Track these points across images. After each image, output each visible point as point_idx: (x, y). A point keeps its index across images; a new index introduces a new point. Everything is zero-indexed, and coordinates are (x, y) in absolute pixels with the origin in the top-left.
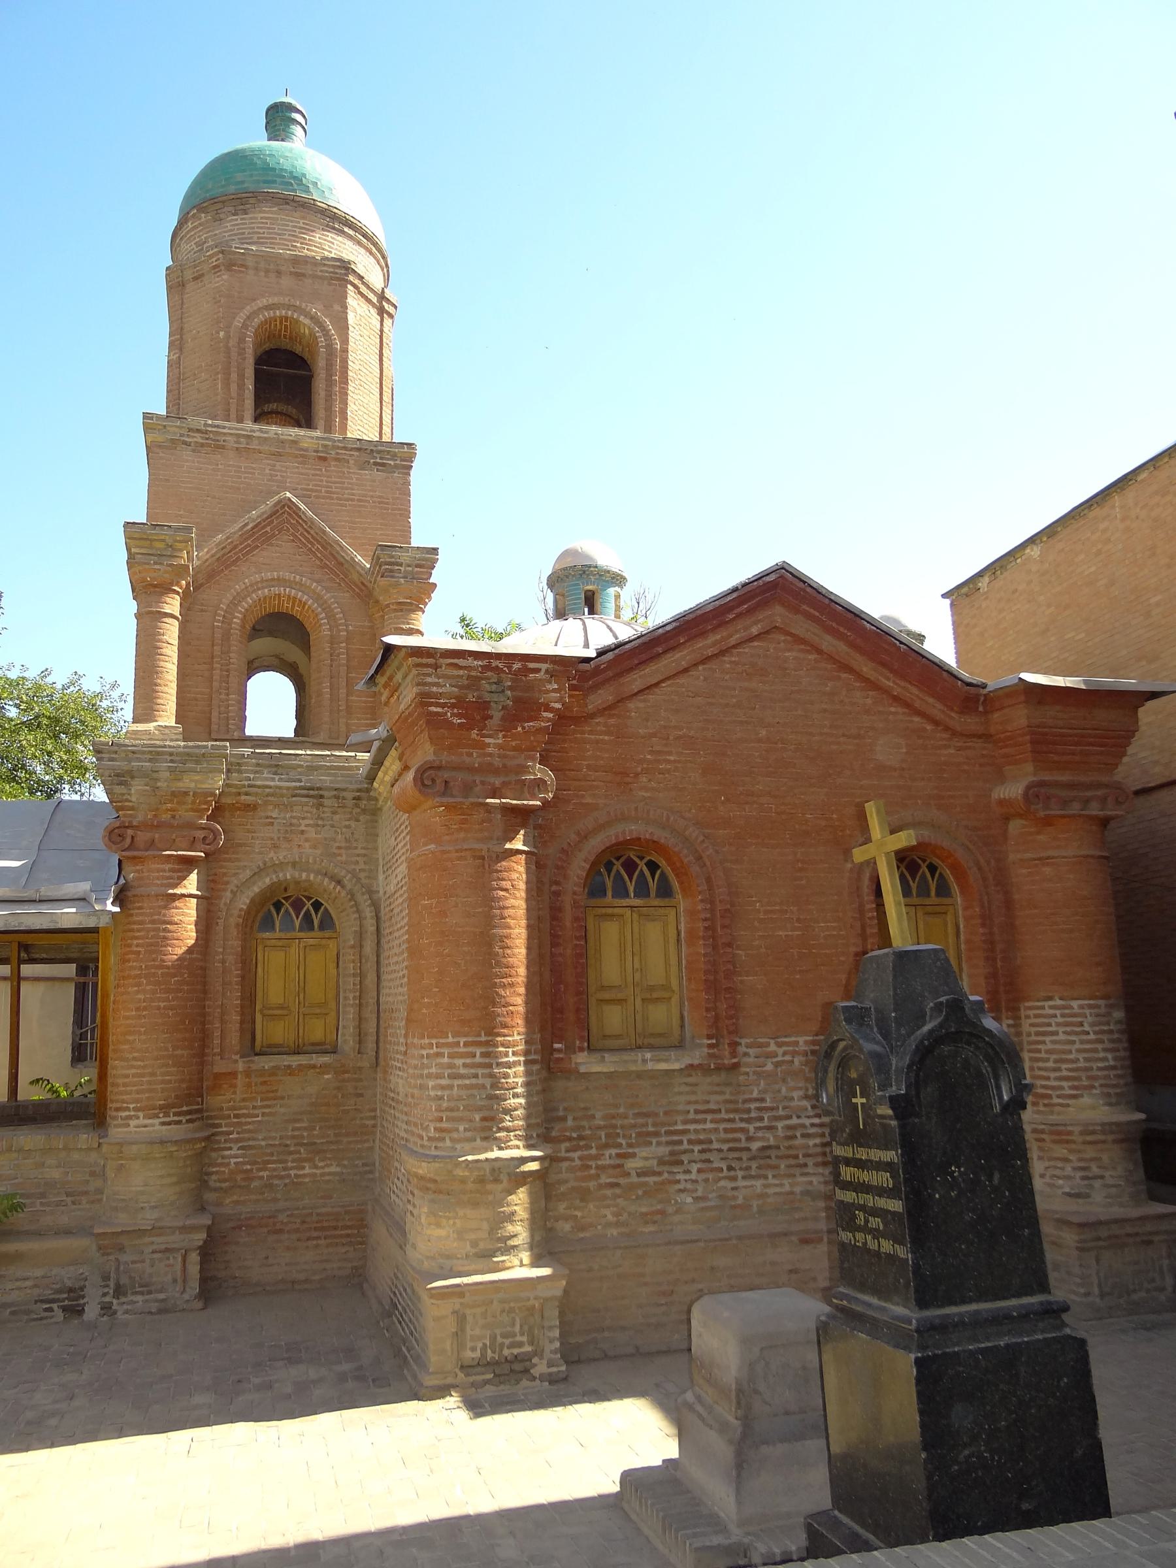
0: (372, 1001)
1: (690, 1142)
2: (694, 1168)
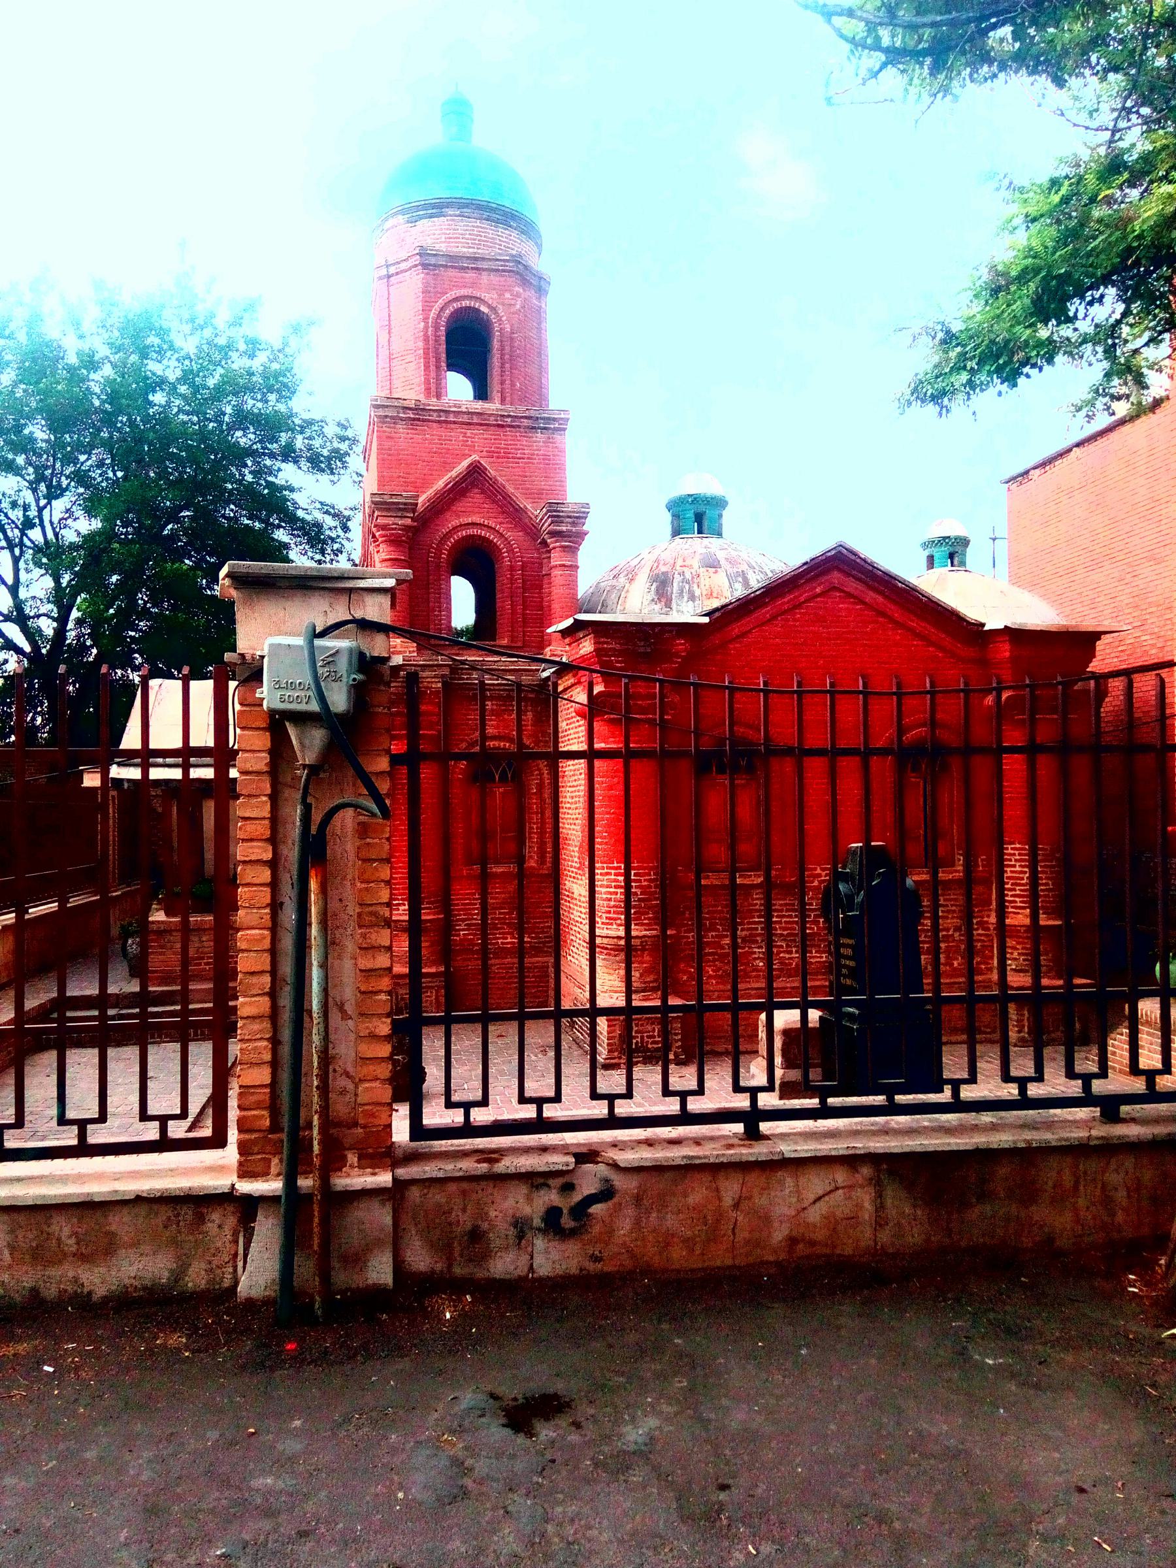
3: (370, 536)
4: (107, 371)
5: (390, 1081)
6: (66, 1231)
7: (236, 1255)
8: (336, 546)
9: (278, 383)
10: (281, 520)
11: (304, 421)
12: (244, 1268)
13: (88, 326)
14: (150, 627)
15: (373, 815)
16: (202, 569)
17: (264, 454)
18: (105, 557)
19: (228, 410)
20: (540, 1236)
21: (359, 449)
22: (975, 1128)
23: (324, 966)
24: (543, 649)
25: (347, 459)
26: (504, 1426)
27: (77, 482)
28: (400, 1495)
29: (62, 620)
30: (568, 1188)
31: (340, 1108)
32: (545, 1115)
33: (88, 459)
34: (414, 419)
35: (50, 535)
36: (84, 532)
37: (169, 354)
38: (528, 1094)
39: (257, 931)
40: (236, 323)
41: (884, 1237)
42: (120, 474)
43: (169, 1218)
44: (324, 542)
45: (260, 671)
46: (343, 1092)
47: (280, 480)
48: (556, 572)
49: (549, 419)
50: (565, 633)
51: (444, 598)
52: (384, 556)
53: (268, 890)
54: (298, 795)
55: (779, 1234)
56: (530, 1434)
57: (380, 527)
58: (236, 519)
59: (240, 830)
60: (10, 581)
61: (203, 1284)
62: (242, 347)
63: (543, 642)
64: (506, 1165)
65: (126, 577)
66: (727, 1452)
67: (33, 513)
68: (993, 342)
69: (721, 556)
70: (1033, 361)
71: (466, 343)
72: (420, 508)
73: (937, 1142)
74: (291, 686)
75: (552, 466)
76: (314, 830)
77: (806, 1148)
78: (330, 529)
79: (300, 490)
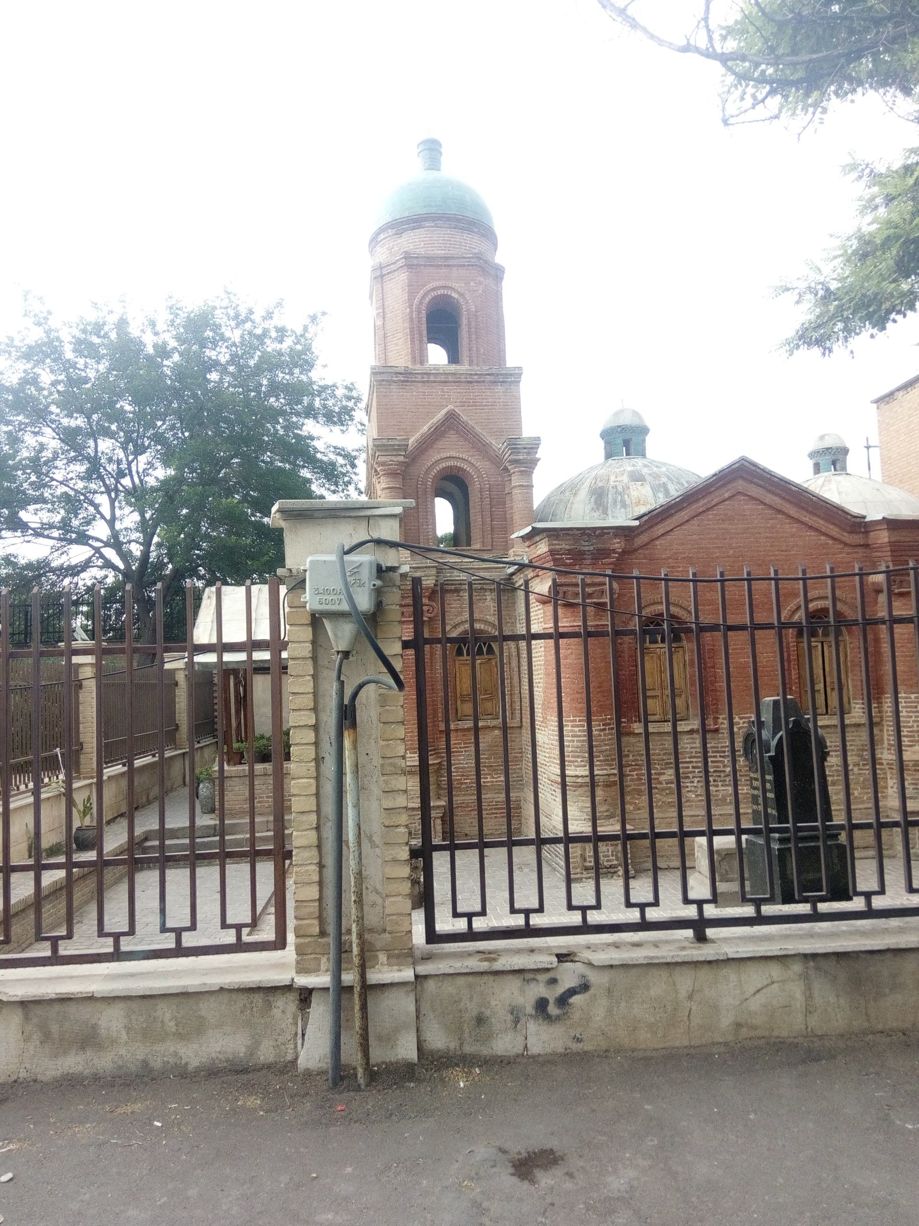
1: (693, 767)
2: (696, 780)
3: (372, 472)
4: (176, 357)
6: (168, 1015)
7: (296, 1034)
8: (346, 479)
9: (302, 359)
10: (305, 462)
11: (320, 386)
12: (303, 1045)
13: (160, 327)
14: (210, 547)
15: (390, 688)
17: (291, 413)
18: (177, 497)
19: (265, 382)
20: (532, 1021)
21: (362, 405)
22: (886, 931)
23: (357, 806)
25: (353, 413)
26: (512, 1175)
27: (156, 442)
29: (147, 544)
32: (531, 923)
33: (163, 424)
34: (404, 381)
36: (161, 478)
37: (220, 344)
40: (269, 316)
41: (813, 1021)
42: (187, 434)
44: (337, 476)
45: (304, 581)
46: (374, 905)
47: (304, 433)
48: (515, 491)
49: (506, 374)
50: (523, 538)
51: (430, 515)
52: (384, 485)
53: (313, 748)
54: (335, 674)
55: (726, 1021)
56: (533, 1182)
57: (383, 464)
58: (272, 463)
60: (108, 517)
61: (271, 1059)
62: (274, 334)
63: (507, 545)
65: (193, 510)
66: (694, 1199)
67: (124, 466)
68: (864, 295)
69: (645, 471)
70: (898, 308)
71: (442, 322)
72: (410, 448)
73: (855, 943)
74: (327, 591)
75: (512, 410)
76: (346, 702)
77: (745, 949)
78: (342, 466)
79: (318, 438)
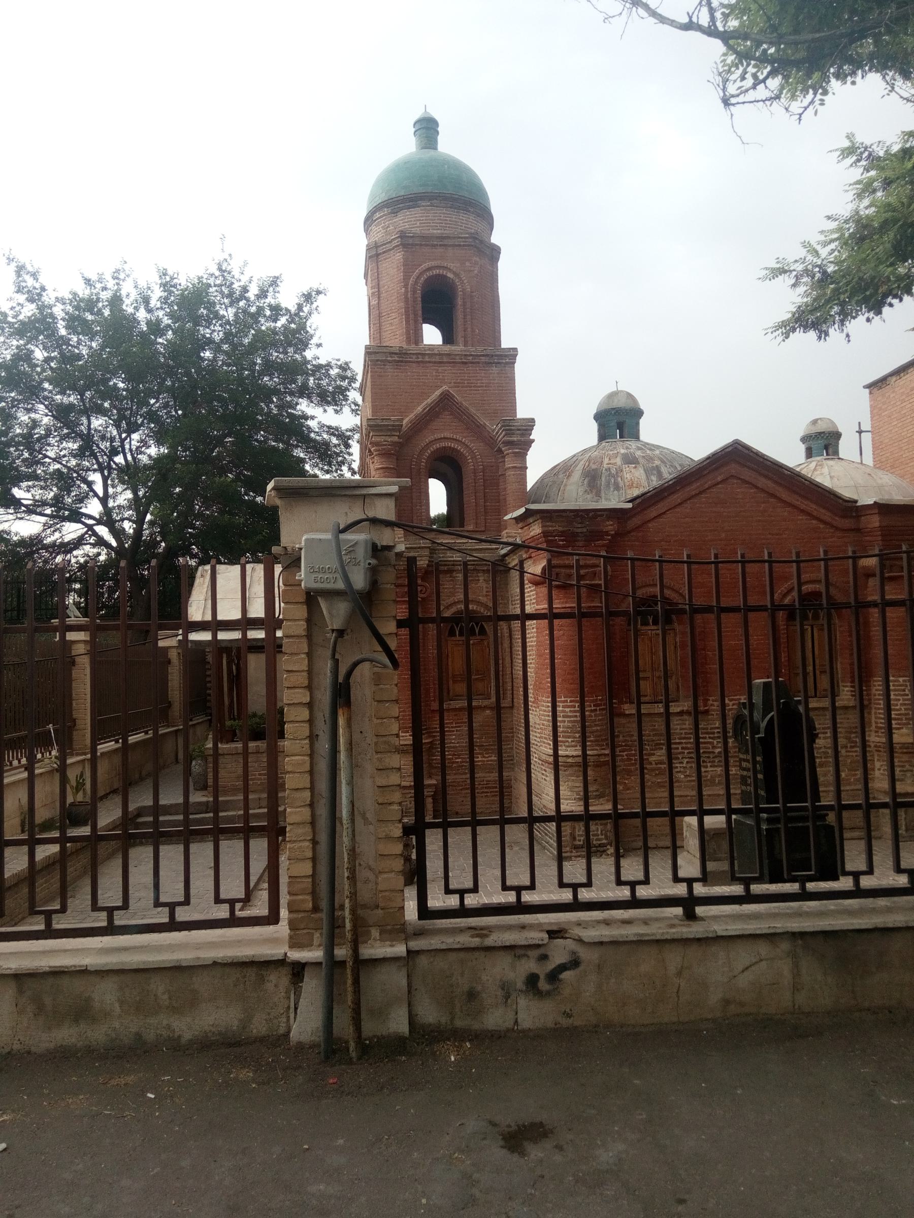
0: (509, 672)
1: (682, 748)
2: (685, 761)
5: (403, 872)
6: (161, 989)
7: (289, 1007)
8: (340, 459)
12: (295, 1018)
15: (385, 666)
16: (241, 481)
22: (874, 911)
23: (350, 783)
24: (501, 532)
25: (348, 393)
26: (502, 1147)
28: (424, 1201)
29: (140, 522)
30: (544, 958)
31: (365, 894)
33: (156, 402)
34: (399, 361)
35: (129, 458)
38: (508, 883)
39: (299, 757)
42: (180, 412)
43: (238, 979)
44: (330, 456)
45: (299, 559)
46: (367, 881)
48: (509, 473)
49: (501, 355)
53: (307, 725)
54: (329, 653)
55: (714, 997)
56: (522, 1154)
57: (374, 444)
59: (284, 679)
63: (500, 526)
64: (493, 940)
68: (861, 279)
70: (895, 292)
72: (404, 428)
73: (842, 922)
74: (322, 570)
76: (341, 680)
77: (734, 927)
